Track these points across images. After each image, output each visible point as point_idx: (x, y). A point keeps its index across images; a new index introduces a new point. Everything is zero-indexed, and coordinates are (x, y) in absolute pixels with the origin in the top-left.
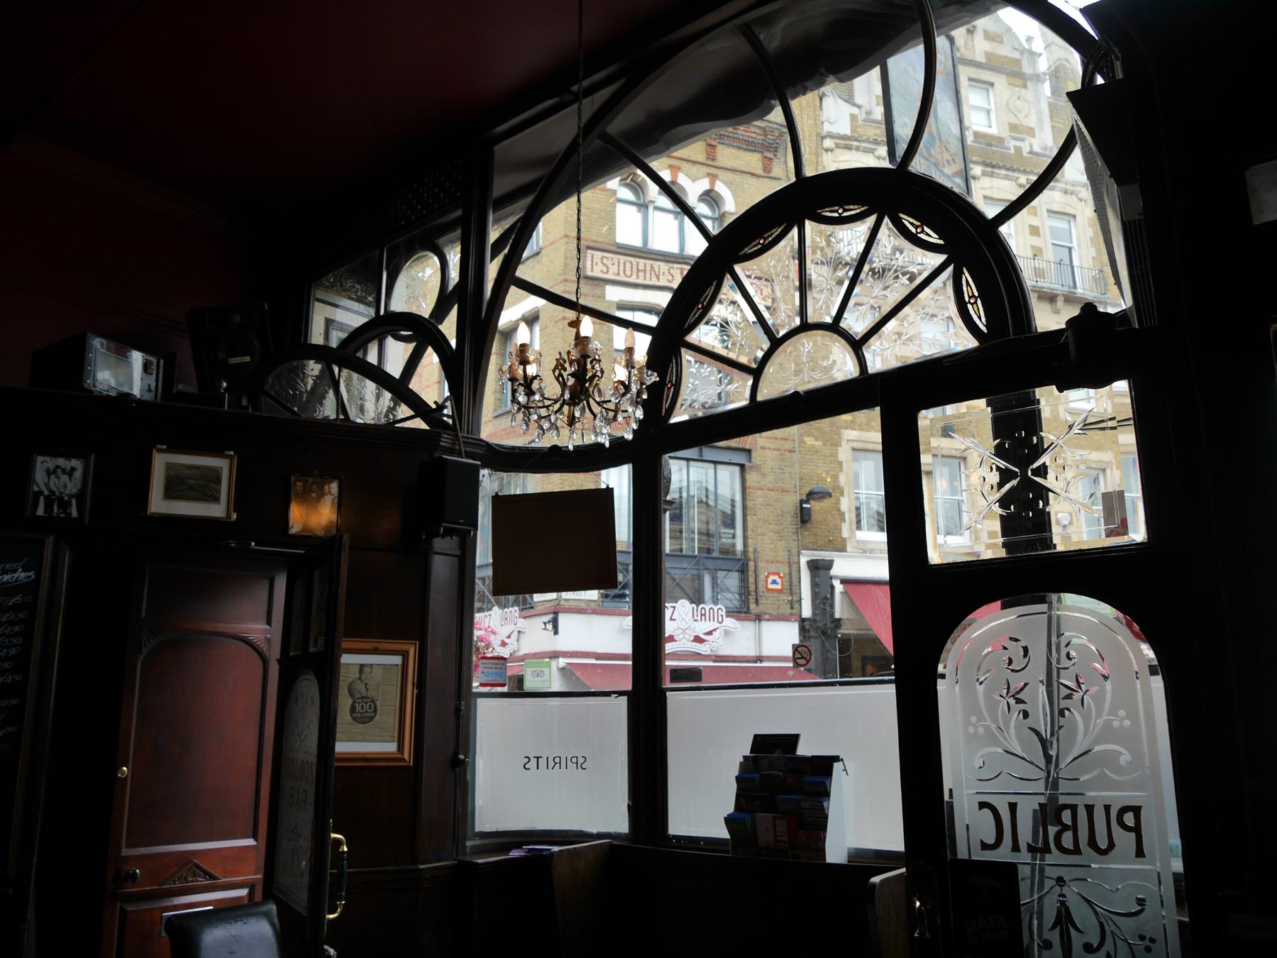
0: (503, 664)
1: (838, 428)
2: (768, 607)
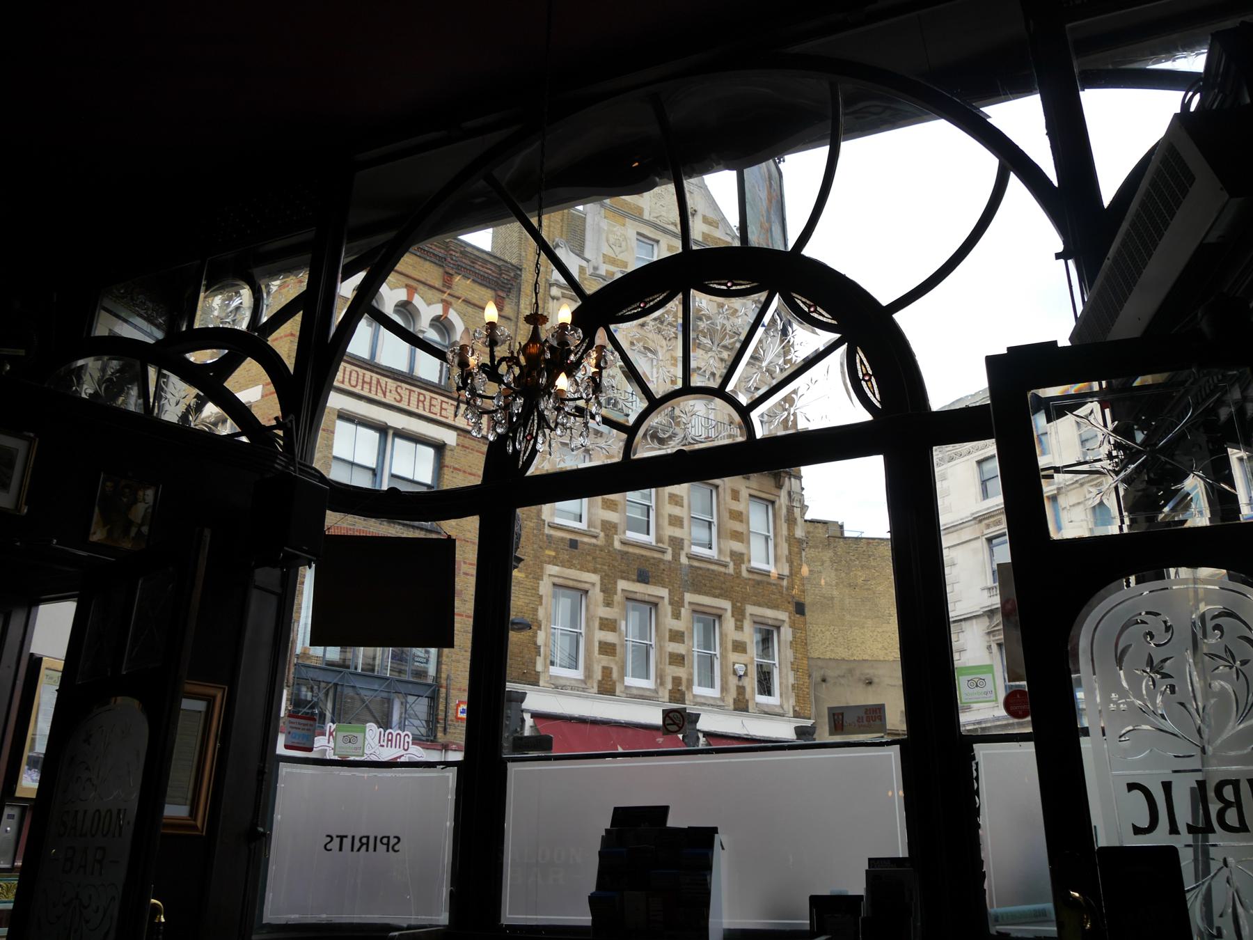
0: (311, 725)
1: (541, 562)
2: (455, 737)
